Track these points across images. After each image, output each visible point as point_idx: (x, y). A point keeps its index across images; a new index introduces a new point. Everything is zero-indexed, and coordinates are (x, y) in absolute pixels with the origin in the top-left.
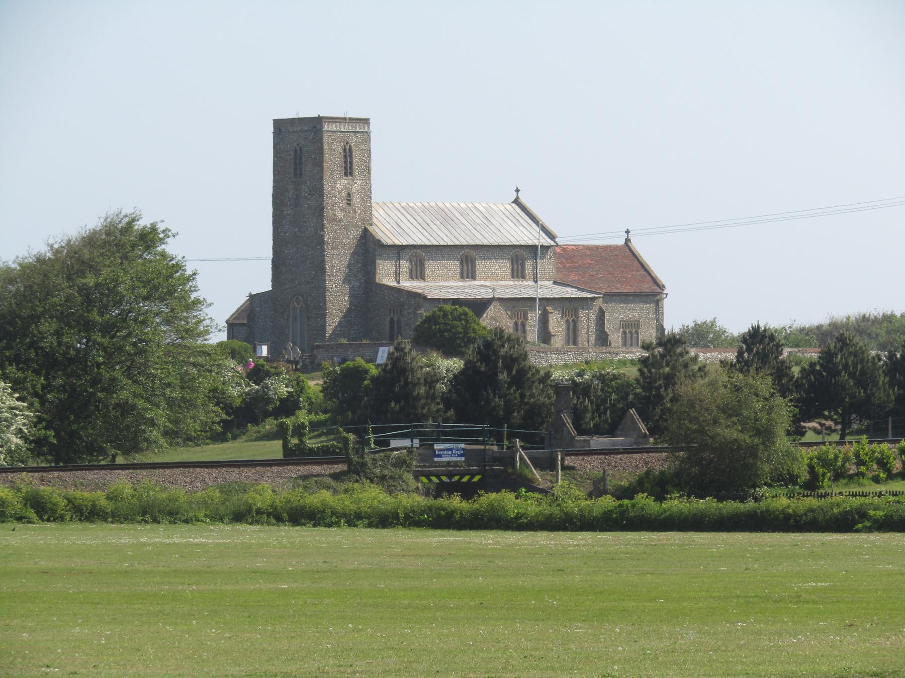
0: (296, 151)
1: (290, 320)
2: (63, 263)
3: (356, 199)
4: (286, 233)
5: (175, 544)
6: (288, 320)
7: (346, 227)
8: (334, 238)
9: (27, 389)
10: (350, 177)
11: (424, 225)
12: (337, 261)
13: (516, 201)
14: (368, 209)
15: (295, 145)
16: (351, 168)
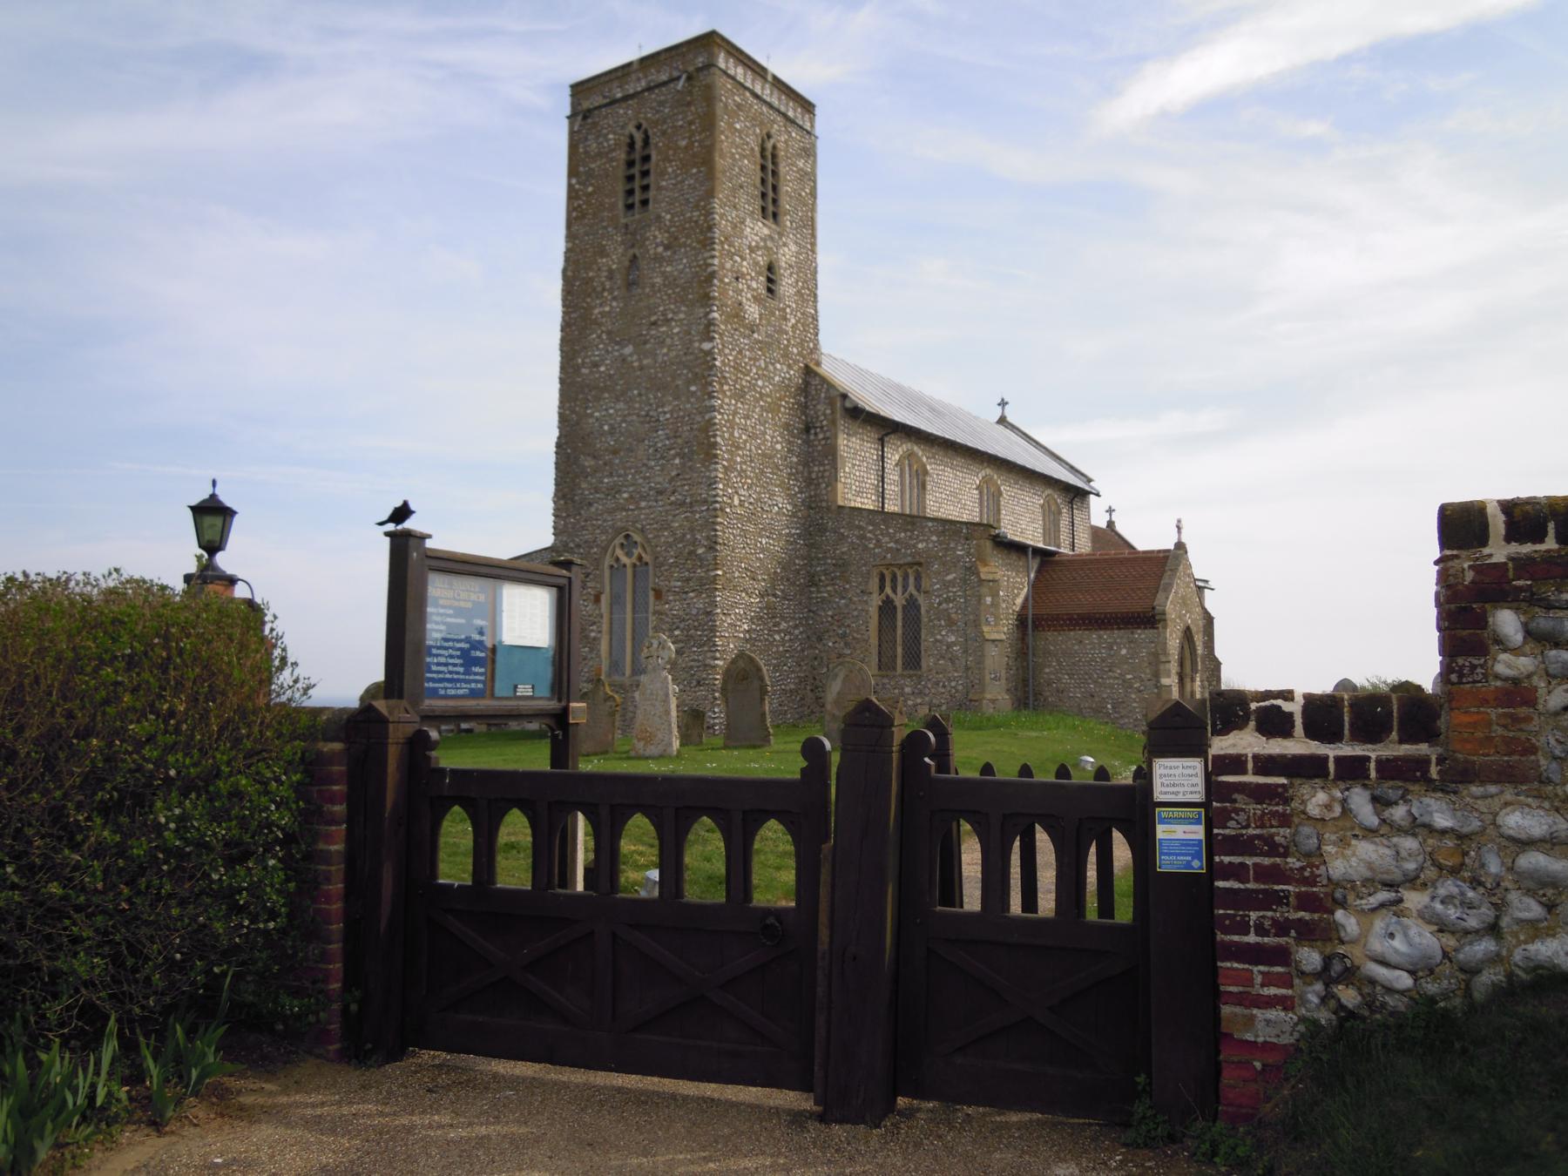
0: (631, 145)
1: (605, 599)
4: (596, 365)
5: (350, 858)
6: (597, 599)
9: (915, 705)
10: (770, 223)
12: (749, 432)
13: (1002, 421)
15: (631, 128)
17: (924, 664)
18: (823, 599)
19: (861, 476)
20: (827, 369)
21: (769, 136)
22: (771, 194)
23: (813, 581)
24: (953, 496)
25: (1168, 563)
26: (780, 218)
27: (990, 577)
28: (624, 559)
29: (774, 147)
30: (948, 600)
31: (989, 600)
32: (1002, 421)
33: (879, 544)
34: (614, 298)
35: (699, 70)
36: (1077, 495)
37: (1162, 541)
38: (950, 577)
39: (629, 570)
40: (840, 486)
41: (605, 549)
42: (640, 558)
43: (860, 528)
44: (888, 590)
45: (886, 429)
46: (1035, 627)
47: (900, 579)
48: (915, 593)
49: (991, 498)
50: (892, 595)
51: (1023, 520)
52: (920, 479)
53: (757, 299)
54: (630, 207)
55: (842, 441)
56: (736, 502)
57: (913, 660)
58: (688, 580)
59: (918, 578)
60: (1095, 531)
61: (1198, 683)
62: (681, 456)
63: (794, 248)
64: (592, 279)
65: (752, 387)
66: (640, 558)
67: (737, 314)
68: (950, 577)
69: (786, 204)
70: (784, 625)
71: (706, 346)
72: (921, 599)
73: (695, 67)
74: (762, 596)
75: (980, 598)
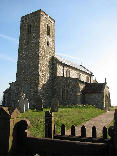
1: (23, 88)
3: (50, 45)
4: (23, 55)
6: (22, 89)
7: (47, 53)
13: (81, 65)
14: (54, 50)
15: (29, 23)
16: (49, 33)
18: (55, 89)
19: (60, 72)
20: (56, 56)
22: (48, 32)
23: (53, 86)
24: (74, 75)
25: (103, 85)
27: (78, 86)
28: (26, 83)
30: (72, 89)
32: (81, 65)
33: (63, 81)
34: (26, 46)
35: (38, 14)
36: (91, 75)
37: (103, 82)
38: (73, 86)
39: (26, 84)
41: (23, 81)
42: (28, 82)
44: (64, 88)
45: (64, 65)
46: (85, 94)
48: (68, 88)
49: (79, 75)
50: (64, 89)
51: (84, 78)
52: (69, 72)
54: (28, 33)
55: (57, 65)
58: (34, 86)
59: (68, 87)
60: (94, 81)
61: (108, 102)
62: (34, 68)
63: (51, 39)
64: (23, 43)
65: (45, 58)
66: (28, 82)
68: (73, 86)
70: (49, 93)
71: (38, 52)
72: (68, 89)
73: (37, 15)
74: (45, 88)
75: (77, 89)
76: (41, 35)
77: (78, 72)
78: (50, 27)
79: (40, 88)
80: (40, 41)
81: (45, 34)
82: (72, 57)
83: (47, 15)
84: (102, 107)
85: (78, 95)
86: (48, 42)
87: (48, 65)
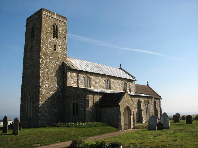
2: (81, 142)
3: (59, 48)
6: (26, 104)
7: (54, 59)
8: (46, 63)
10: (56, 38)
11: (90, 67)
15: (33, 25)
16: (57, 35)
17: (79, 114)
19: (72, 81)
21: (55, 24)
26: (58, 37)
27: (87, 98)
29: (57, 25)
31: (87, 102)
40: (68, 82)
43: (70, 90)
44: (74, 101)
47: (76, 99)
53: (51, 51)
56: (45, 86)
57: (77, 114)
67: (46, 54)
69: (59, 35)
70: (57, 107)
72: (78, 102)
73: (38, 16)
76: (43, 38)
77: (105, 79)
78: (58, 26)
79: (43, 103)
80: (41, 46)
81: (50, 37)
82: (150, 53)
83: (54, 14)
84: (118, 124)
85: (86, 109)
86: (55, 45)
87: (54, 74)
